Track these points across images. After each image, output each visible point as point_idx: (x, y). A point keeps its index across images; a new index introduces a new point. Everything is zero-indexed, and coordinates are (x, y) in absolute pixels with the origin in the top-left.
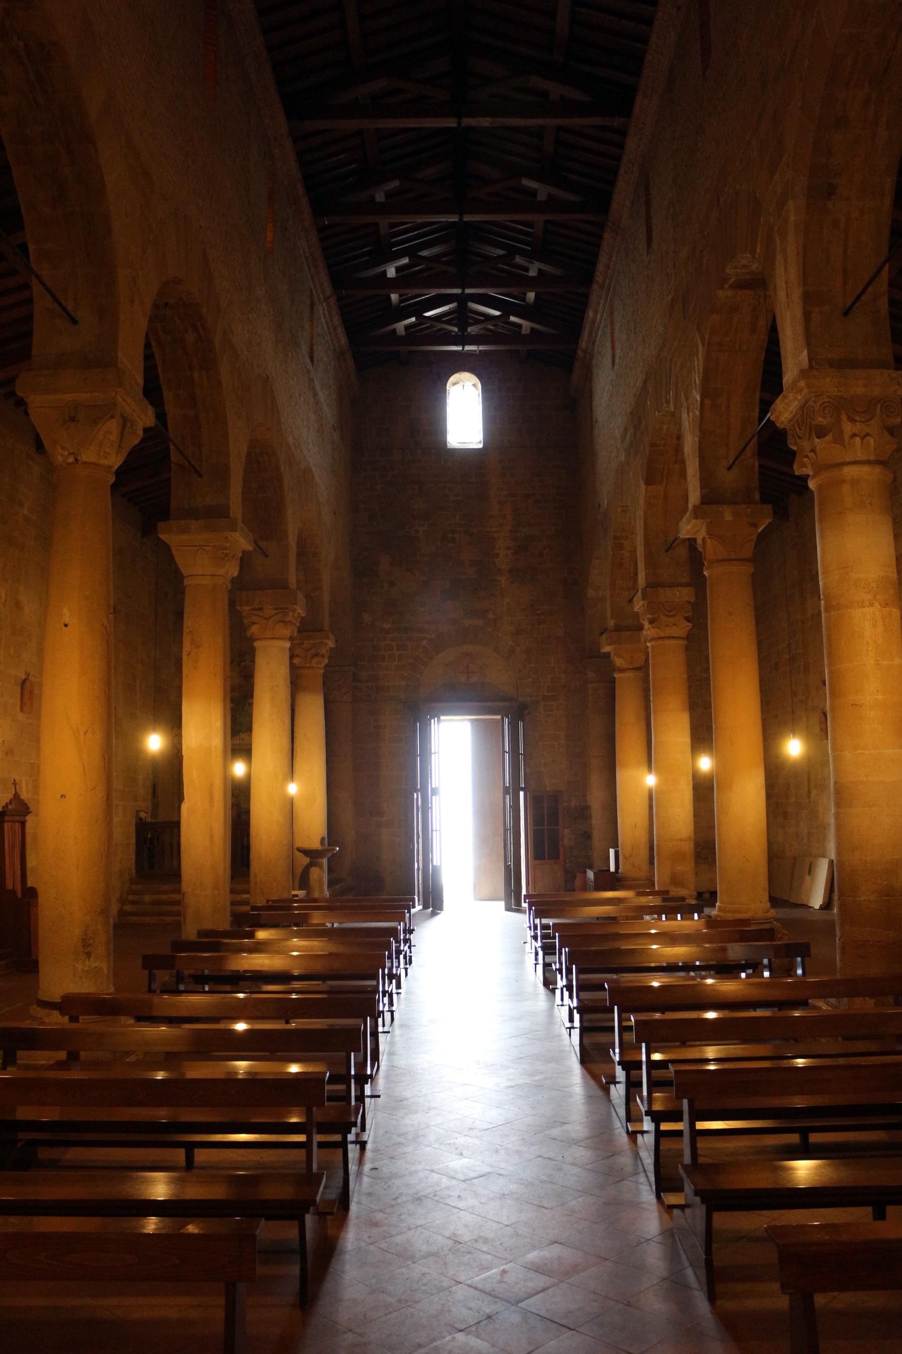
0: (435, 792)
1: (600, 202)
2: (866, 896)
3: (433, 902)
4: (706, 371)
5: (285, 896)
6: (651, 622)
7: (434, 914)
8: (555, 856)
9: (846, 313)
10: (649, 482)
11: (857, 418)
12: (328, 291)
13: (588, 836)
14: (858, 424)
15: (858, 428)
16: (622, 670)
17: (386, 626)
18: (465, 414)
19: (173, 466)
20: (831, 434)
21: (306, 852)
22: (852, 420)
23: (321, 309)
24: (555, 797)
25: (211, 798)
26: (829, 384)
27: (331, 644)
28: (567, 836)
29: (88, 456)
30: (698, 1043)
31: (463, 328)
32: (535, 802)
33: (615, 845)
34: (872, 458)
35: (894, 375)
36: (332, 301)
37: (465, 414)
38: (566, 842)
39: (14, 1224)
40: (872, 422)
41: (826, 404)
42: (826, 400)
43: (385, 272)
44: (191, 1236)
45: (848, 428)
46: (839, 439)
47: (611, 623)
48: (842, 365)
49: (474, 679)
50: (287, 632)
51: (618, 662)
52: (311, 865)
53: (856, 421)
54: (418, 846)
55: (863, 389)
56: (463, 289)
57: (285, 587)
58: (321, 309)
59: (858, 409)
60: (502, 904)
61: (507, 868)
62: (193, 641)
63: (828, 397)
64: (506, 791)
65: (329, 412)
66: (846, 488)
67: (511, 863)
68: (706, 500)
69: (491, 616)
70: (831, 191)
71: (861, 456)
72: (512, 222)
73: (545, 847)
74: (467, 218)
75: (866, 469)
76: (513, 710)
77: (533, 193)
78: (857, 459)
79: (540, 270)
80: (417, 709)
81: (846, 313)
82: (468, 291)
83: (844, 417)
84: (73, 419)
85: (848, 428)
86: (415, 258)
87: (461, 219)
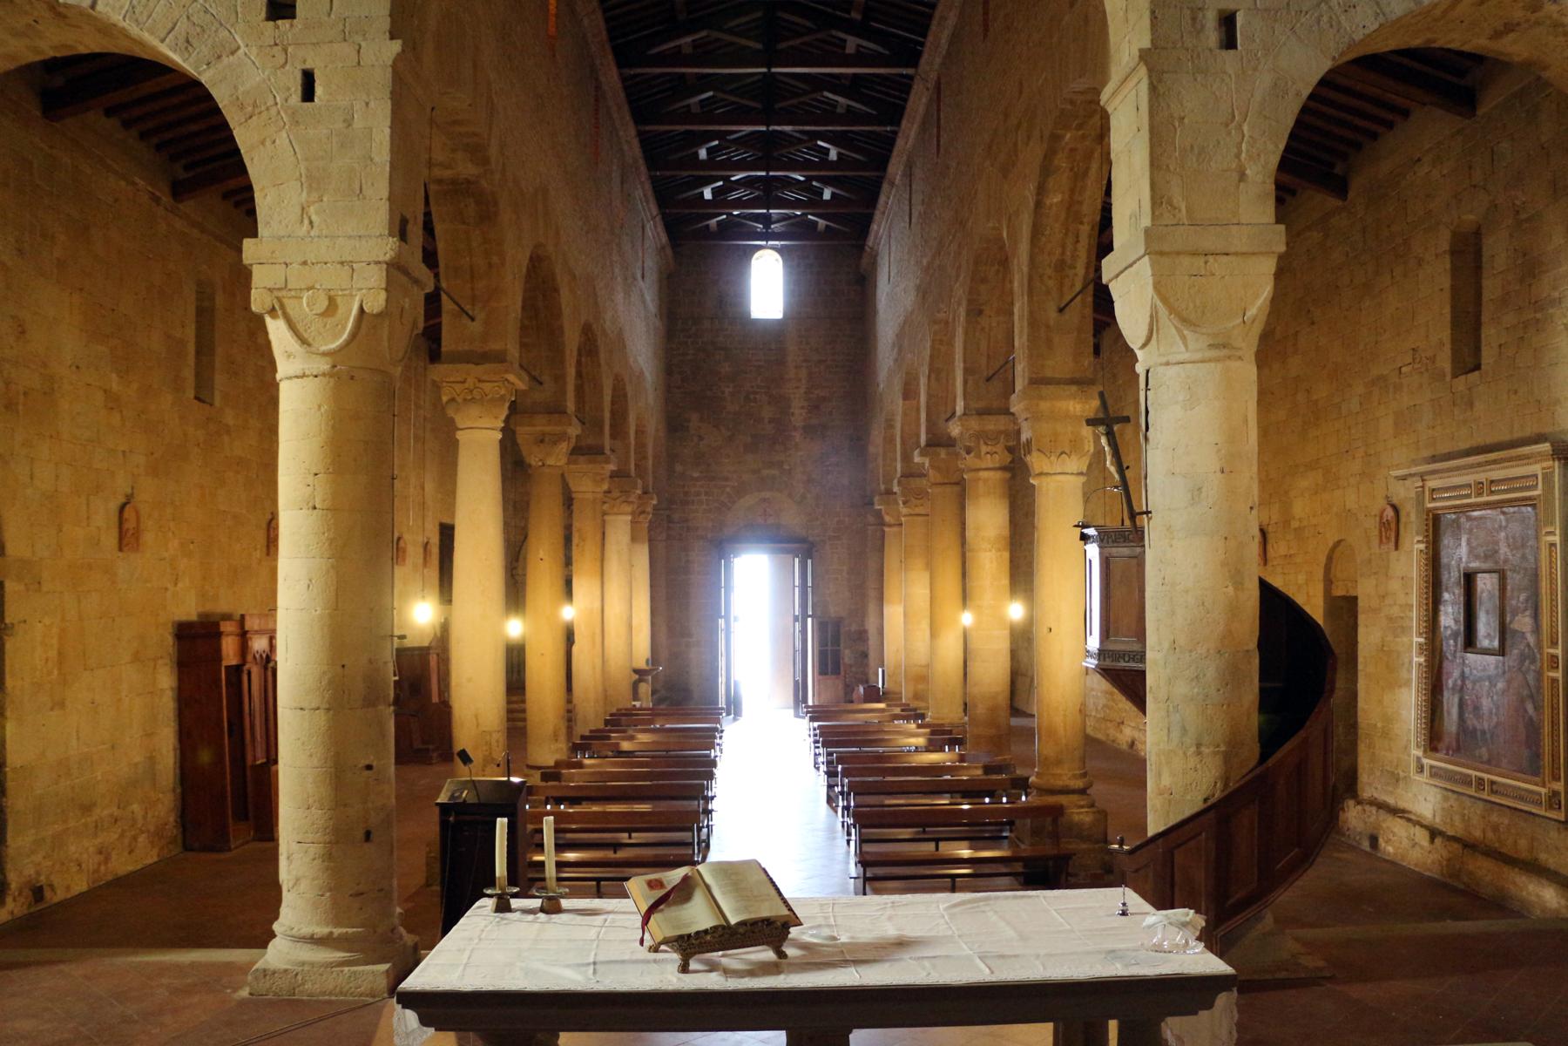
0: (736, 619)
1: (882, 163)
3: (734, 708)
4: (931, 356)
6: (905, 503)
7: (735, 719)
8: (836, 671)
9: (988, 380)
10: (905, 398)
13: (865, 655)
15: (989, 449)
16: (890, 526)
17: (696, 475)
18: (767, 285)
19: (514, 352)
21: (636, 671)
24: (838, 623)
26: (974, 424)
27: (655, 502)
28: (847, 656)
29: (551, 461)
31: (767, 226)
32: (822, 627)
33: (882, 666)
36: (658, 219)
37: (767, 285)
38: (847, 660)
43: (696, 154)
45: (984, 449)
46: (978, 456)
47: (883, 487)
48: (982, 413)
49: (771, 521)
50: (629, 509)
52: (640, 680)
54: (722, 663)
57: (629, 476)
58: (649, 226)
60: (792, 712)
61: (796, 683)
64: (796, 619)
65: (652, 307)
66: (981, 483)
67: (799, 678)
68: (928, 445)
70: (980, 312)
73: (829, 664)
76: (801, 546)
77: (834, 105)
79: (833, 194)
80: (721, 545)
81: (988, 380)
85: (984, 449)
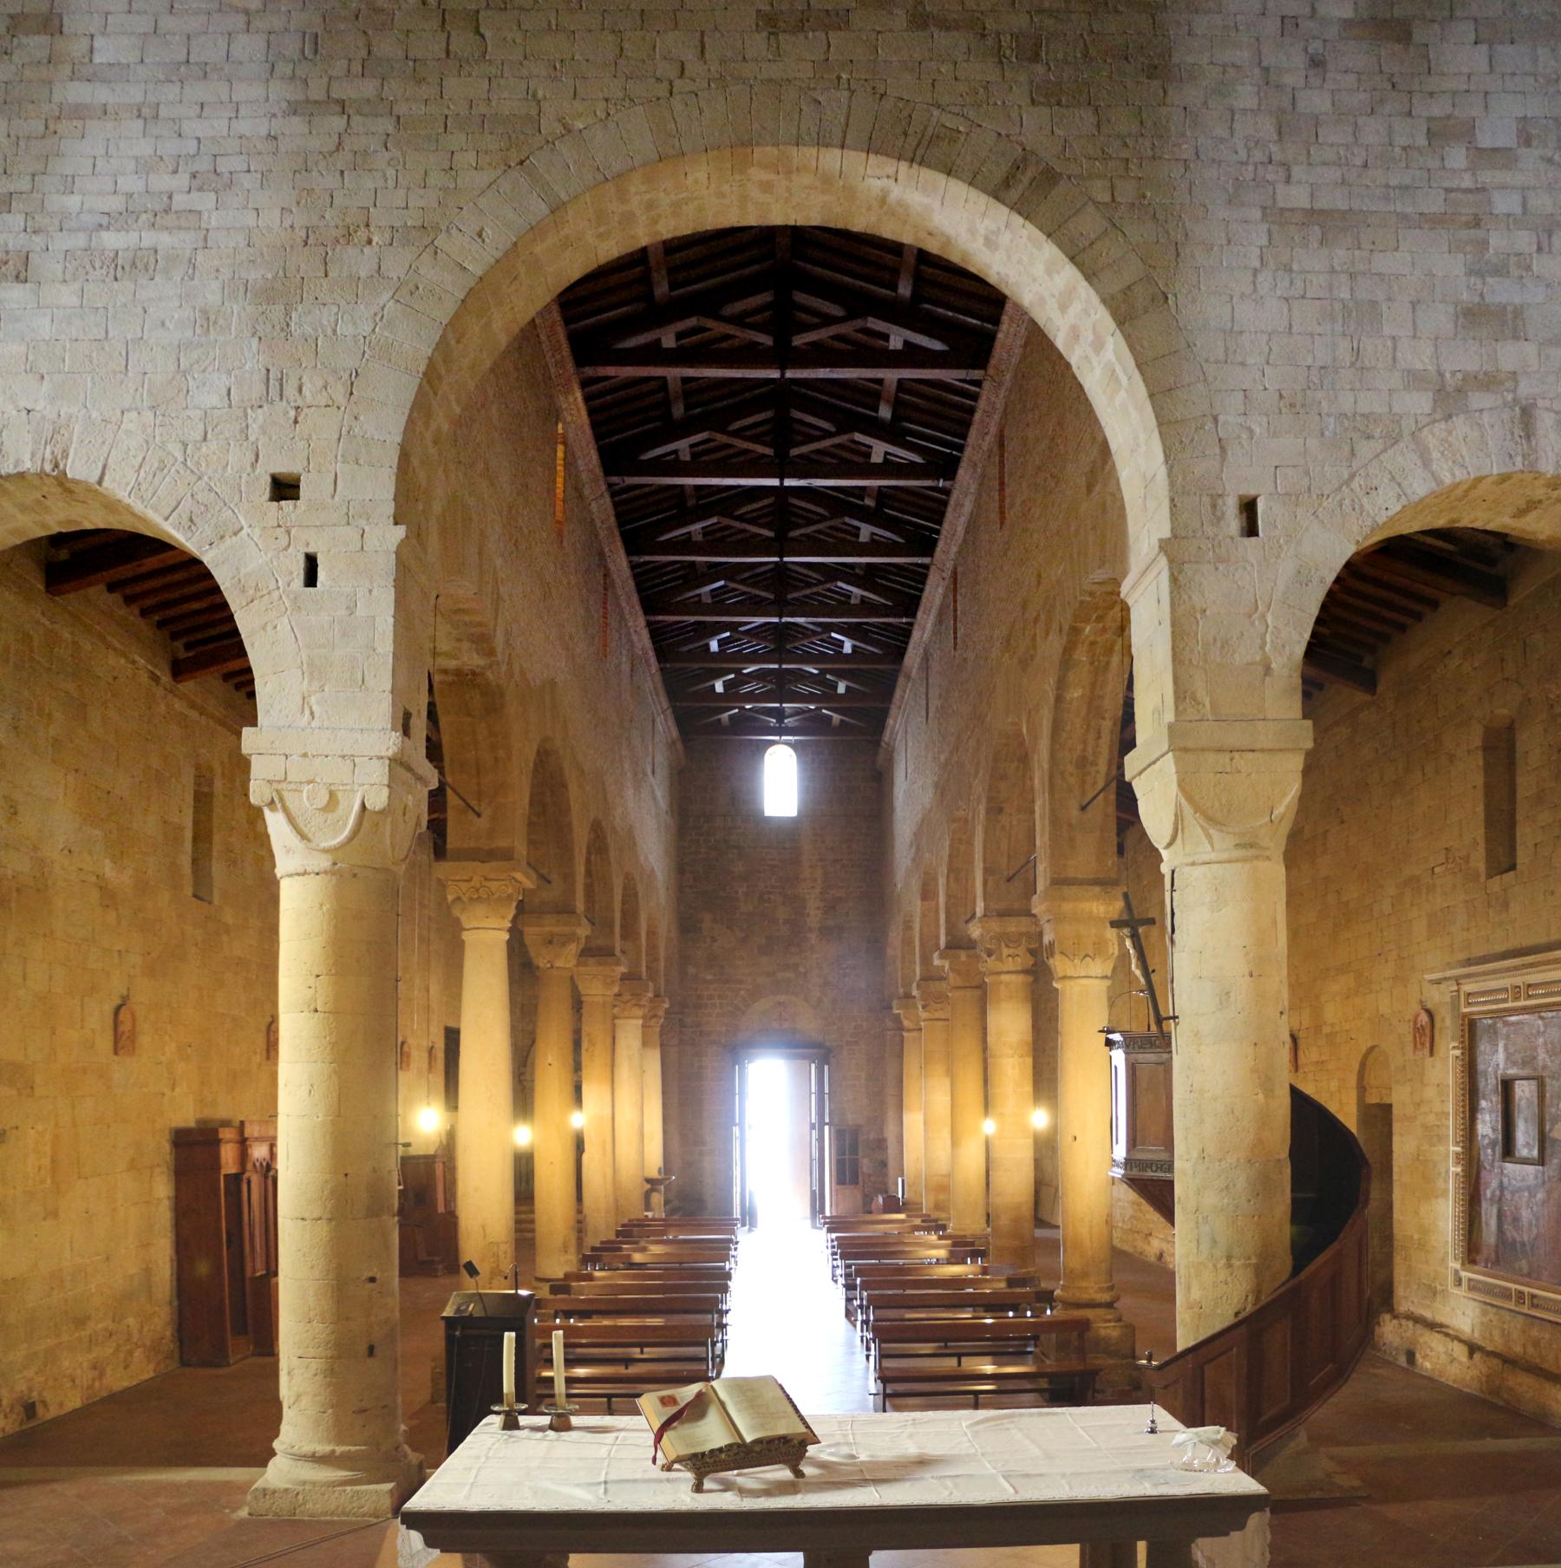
2: (1004, 1221)
5: (641, 1216)
12: (665, 705)
13: (884, 1164)
15: (1011, 951)
17: (709, 977)
18: (780, 781)
21: (648, 1181)
23: (660, 719)
24: (856, 1131)
25: (604, 1149)
26: (995, 926)
28: (866, 1165)
36: (669, 712)
37: (780, 781)
38: (865, 1169)
43: (707, 646)
45: (1006, 951)
46: (1000, 959)
48: (1002, 914)
49: (786, 1025)
50: (640, 1012)
51: (906, 1023)
52: (652, 1190)
54: (737, 1173)
56: (781, 557)
58: (660, 719)
61: (813, 1193)
62: (590, 1041)
64: (812, 1127)
65: (663, 804)
66: (1002, 987)
68: (949, 947)
69: (802, 969)
71: (1012, 968)
73: (847, 1173)
74: (789, 374)
75: (1013, 977)
77: (848, 596)
80: (735, 1050)
81: (1009, 880)
82: (788, 482)
84: (551, 942)
85: (1006, 951)
86: (738, 672)
87: (783, 374)
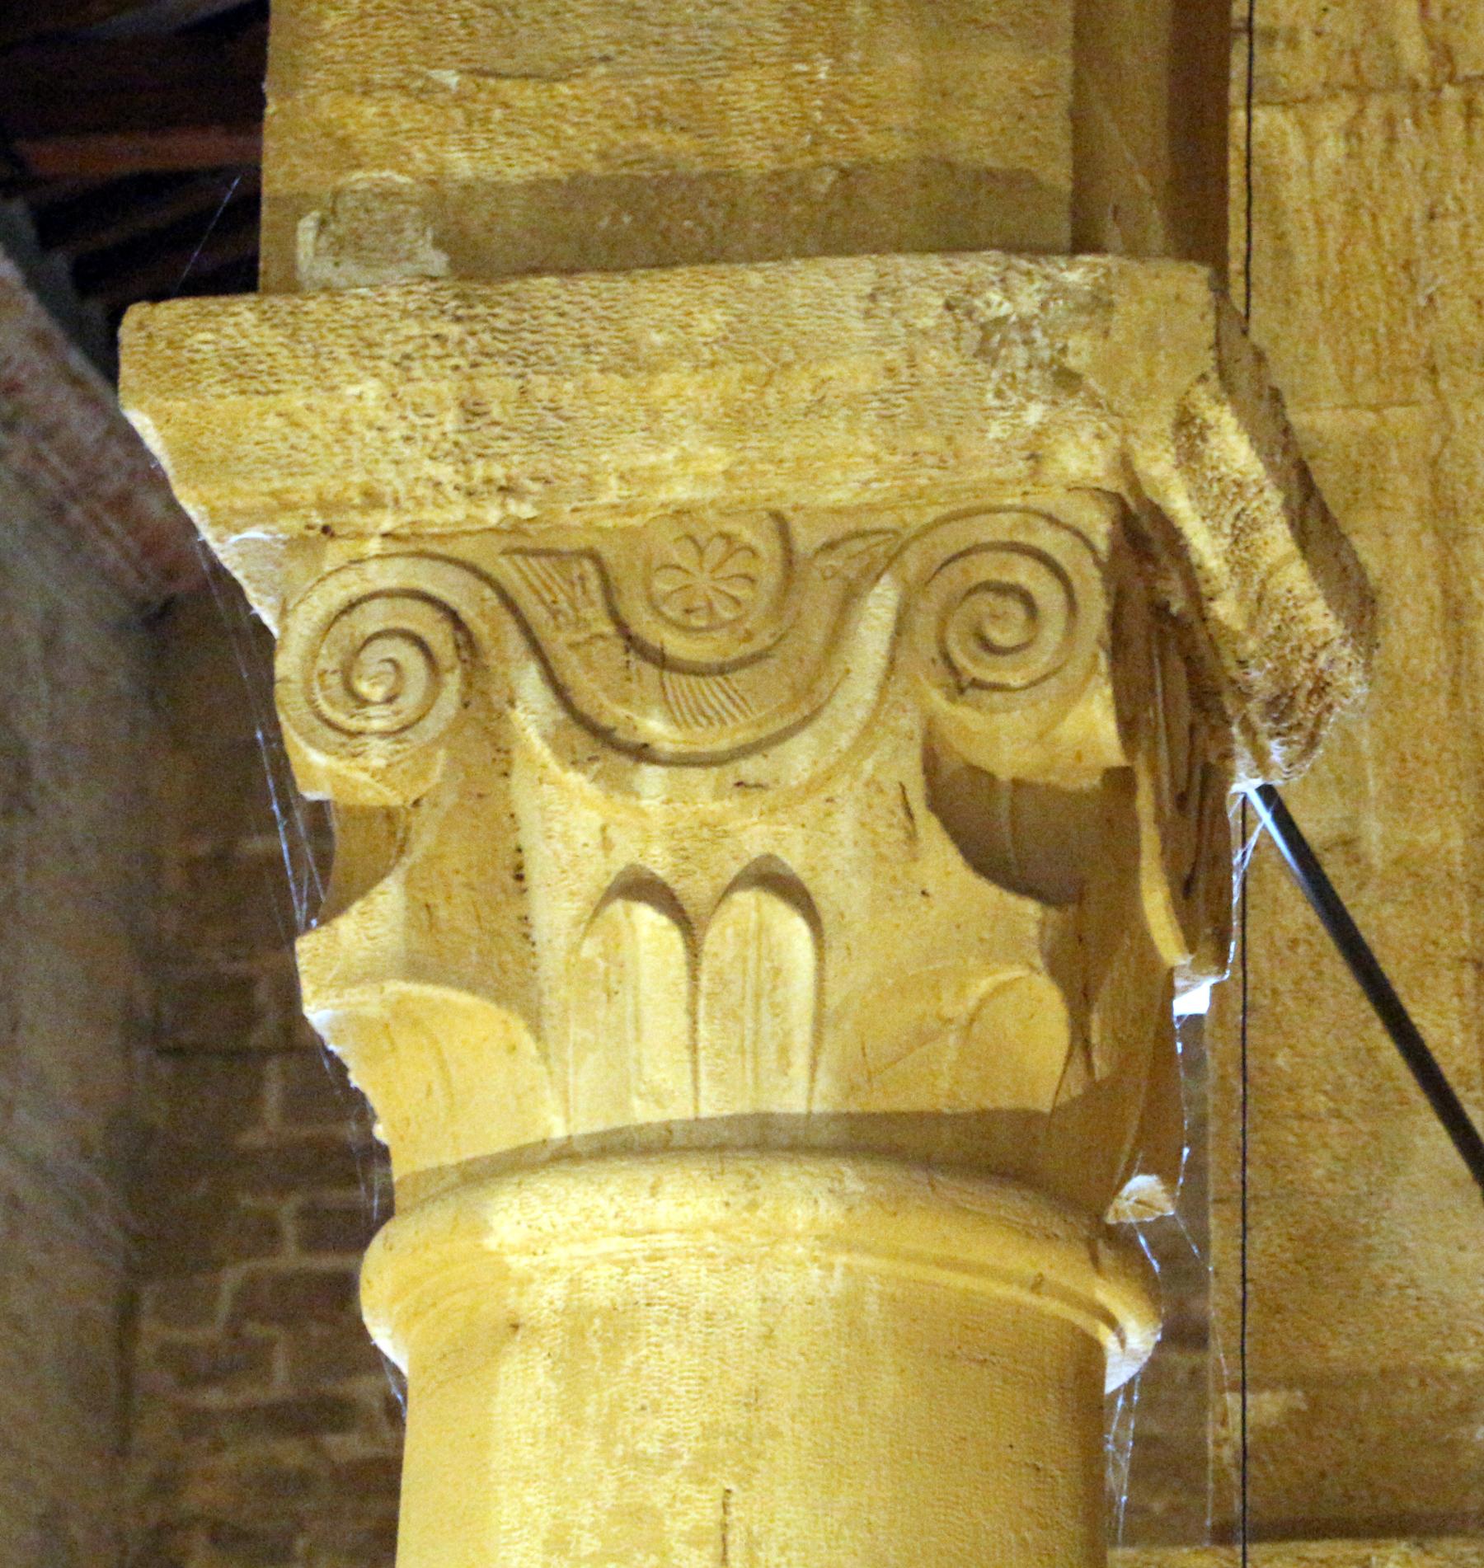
11: (655, 727)
14: (651, 778)
15: (650, 818)
20: (388, 899)
22: (601, 743)
30: (1235, 168)
34: (798, 1094)
35: (995, 303)
39: (736, 1553)
40: (799, 758)
41: (374, 618)
42: (389, 575)
44: (1183, 1048)
45: (573, 822)
53: (643, 753)
55: (716, 458)
59: (676, 645)
63: (408, 543)
71: (670, 1092)
72: (311, 878)
78: (643, 1113)
83: (531, 713)
85: (573, 822)
